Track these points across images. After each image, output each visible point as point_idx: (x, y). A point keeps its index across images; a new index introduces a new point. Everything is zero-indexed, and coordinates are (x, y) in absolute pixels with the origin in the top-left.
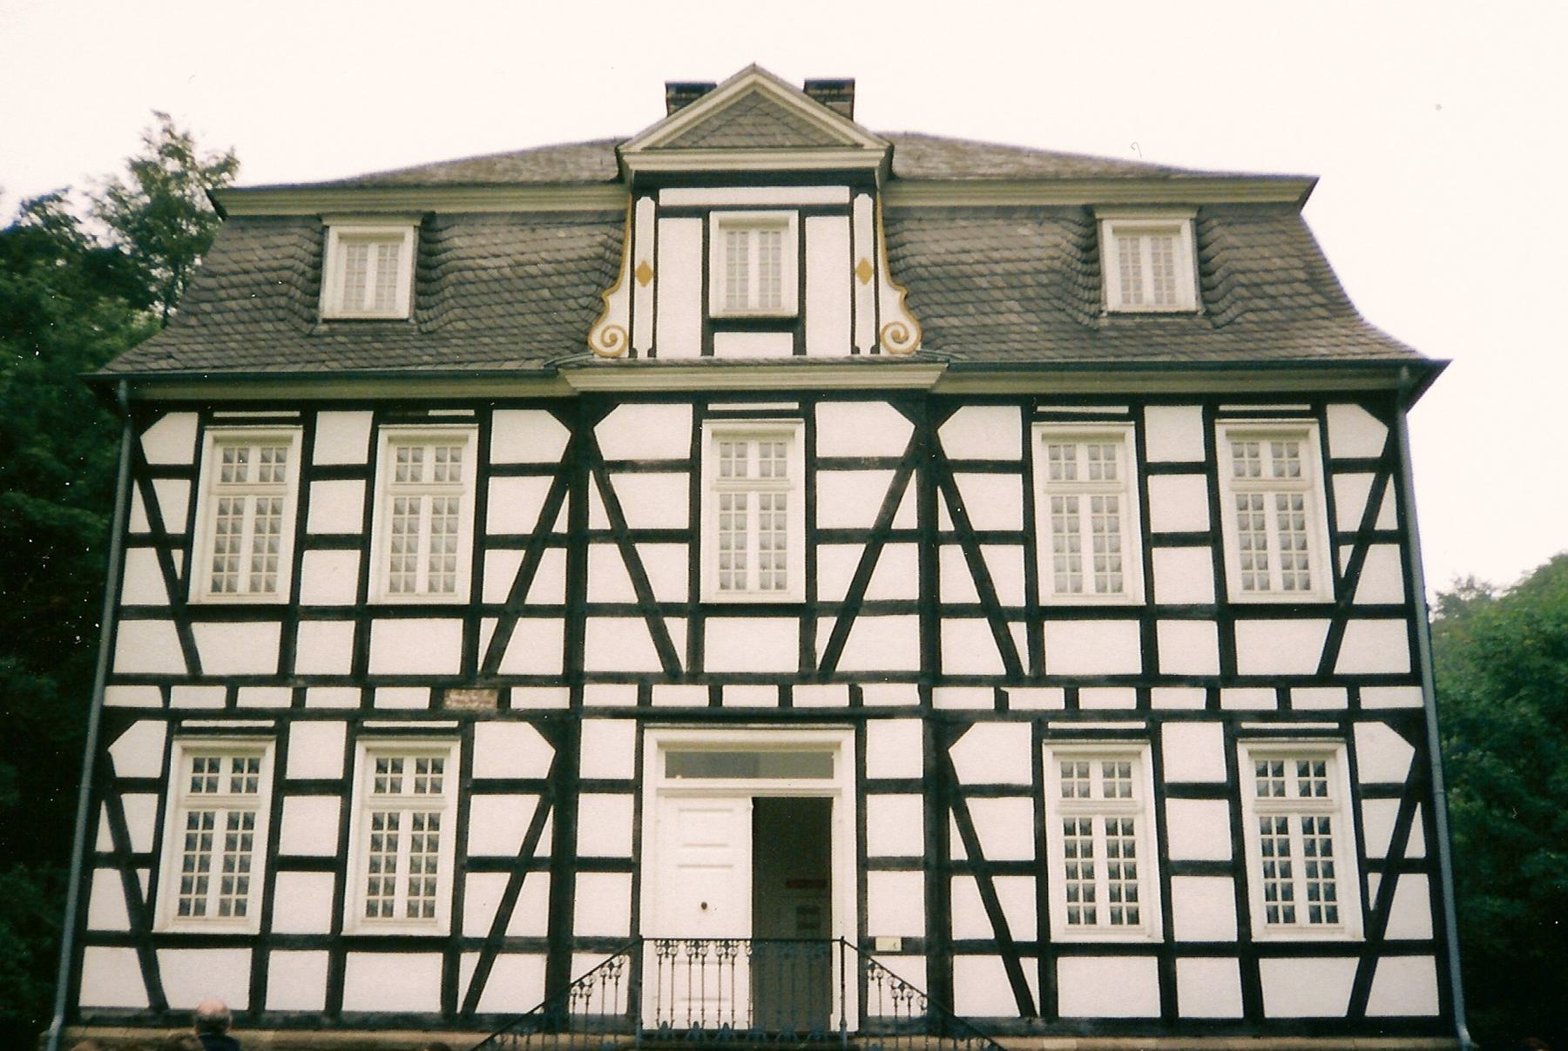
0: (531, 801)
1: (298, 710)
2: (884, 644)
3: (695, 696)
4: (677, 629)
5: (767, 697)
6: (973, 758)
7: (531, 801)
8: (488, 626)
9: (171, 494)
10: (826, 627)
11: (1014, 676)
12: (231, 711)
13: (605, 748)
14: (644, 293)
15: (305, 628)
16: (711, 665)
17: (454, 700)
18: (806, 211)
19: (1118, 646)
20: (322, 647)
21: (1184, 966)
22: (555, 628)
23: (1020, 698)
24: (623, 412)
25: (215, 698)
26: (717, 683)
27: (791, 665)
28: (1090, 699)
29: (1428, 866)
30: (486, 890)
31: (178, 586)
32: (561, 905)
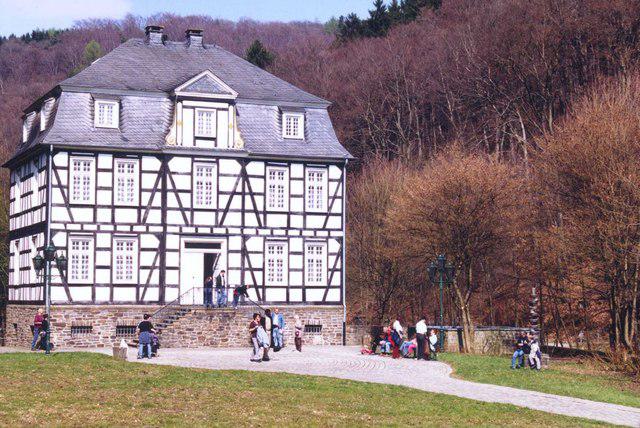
0: (156, 175)
1: (99, 231)
2: (233, 219)
3: (192, 230)
4: (188, 214)
5: (208, 231)
6: (251, 245)
7: (155, 253)
8: (143, 211)
9: (62, 174)
10: (221, 214)
11: (260, 227)
12: (82, 230)
13: (172, 242)
14: (179, 128)
15: (99, 210)
16: (195, 223)
17: (136, 229)
18: (218, 109)
19: (282, 221)
20: (104, 215)
21: (291, 290)
22: (159, 213)
23: (261, 232)
24: (175, 159)
25: (78, 227)
26: (197, 227)
27: (213, 223)
28: (276, 232)
29: (342, 198)
30: (145, 274)
31: (67, 199)
32: (162, 278)
